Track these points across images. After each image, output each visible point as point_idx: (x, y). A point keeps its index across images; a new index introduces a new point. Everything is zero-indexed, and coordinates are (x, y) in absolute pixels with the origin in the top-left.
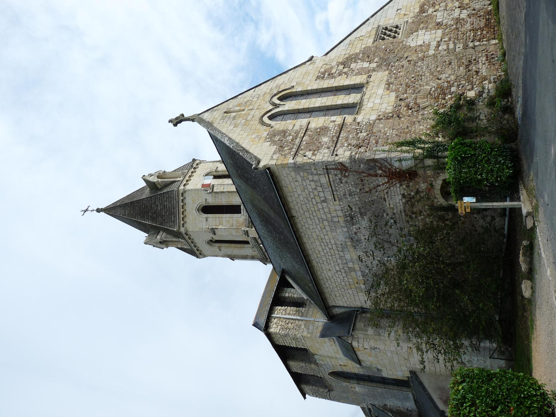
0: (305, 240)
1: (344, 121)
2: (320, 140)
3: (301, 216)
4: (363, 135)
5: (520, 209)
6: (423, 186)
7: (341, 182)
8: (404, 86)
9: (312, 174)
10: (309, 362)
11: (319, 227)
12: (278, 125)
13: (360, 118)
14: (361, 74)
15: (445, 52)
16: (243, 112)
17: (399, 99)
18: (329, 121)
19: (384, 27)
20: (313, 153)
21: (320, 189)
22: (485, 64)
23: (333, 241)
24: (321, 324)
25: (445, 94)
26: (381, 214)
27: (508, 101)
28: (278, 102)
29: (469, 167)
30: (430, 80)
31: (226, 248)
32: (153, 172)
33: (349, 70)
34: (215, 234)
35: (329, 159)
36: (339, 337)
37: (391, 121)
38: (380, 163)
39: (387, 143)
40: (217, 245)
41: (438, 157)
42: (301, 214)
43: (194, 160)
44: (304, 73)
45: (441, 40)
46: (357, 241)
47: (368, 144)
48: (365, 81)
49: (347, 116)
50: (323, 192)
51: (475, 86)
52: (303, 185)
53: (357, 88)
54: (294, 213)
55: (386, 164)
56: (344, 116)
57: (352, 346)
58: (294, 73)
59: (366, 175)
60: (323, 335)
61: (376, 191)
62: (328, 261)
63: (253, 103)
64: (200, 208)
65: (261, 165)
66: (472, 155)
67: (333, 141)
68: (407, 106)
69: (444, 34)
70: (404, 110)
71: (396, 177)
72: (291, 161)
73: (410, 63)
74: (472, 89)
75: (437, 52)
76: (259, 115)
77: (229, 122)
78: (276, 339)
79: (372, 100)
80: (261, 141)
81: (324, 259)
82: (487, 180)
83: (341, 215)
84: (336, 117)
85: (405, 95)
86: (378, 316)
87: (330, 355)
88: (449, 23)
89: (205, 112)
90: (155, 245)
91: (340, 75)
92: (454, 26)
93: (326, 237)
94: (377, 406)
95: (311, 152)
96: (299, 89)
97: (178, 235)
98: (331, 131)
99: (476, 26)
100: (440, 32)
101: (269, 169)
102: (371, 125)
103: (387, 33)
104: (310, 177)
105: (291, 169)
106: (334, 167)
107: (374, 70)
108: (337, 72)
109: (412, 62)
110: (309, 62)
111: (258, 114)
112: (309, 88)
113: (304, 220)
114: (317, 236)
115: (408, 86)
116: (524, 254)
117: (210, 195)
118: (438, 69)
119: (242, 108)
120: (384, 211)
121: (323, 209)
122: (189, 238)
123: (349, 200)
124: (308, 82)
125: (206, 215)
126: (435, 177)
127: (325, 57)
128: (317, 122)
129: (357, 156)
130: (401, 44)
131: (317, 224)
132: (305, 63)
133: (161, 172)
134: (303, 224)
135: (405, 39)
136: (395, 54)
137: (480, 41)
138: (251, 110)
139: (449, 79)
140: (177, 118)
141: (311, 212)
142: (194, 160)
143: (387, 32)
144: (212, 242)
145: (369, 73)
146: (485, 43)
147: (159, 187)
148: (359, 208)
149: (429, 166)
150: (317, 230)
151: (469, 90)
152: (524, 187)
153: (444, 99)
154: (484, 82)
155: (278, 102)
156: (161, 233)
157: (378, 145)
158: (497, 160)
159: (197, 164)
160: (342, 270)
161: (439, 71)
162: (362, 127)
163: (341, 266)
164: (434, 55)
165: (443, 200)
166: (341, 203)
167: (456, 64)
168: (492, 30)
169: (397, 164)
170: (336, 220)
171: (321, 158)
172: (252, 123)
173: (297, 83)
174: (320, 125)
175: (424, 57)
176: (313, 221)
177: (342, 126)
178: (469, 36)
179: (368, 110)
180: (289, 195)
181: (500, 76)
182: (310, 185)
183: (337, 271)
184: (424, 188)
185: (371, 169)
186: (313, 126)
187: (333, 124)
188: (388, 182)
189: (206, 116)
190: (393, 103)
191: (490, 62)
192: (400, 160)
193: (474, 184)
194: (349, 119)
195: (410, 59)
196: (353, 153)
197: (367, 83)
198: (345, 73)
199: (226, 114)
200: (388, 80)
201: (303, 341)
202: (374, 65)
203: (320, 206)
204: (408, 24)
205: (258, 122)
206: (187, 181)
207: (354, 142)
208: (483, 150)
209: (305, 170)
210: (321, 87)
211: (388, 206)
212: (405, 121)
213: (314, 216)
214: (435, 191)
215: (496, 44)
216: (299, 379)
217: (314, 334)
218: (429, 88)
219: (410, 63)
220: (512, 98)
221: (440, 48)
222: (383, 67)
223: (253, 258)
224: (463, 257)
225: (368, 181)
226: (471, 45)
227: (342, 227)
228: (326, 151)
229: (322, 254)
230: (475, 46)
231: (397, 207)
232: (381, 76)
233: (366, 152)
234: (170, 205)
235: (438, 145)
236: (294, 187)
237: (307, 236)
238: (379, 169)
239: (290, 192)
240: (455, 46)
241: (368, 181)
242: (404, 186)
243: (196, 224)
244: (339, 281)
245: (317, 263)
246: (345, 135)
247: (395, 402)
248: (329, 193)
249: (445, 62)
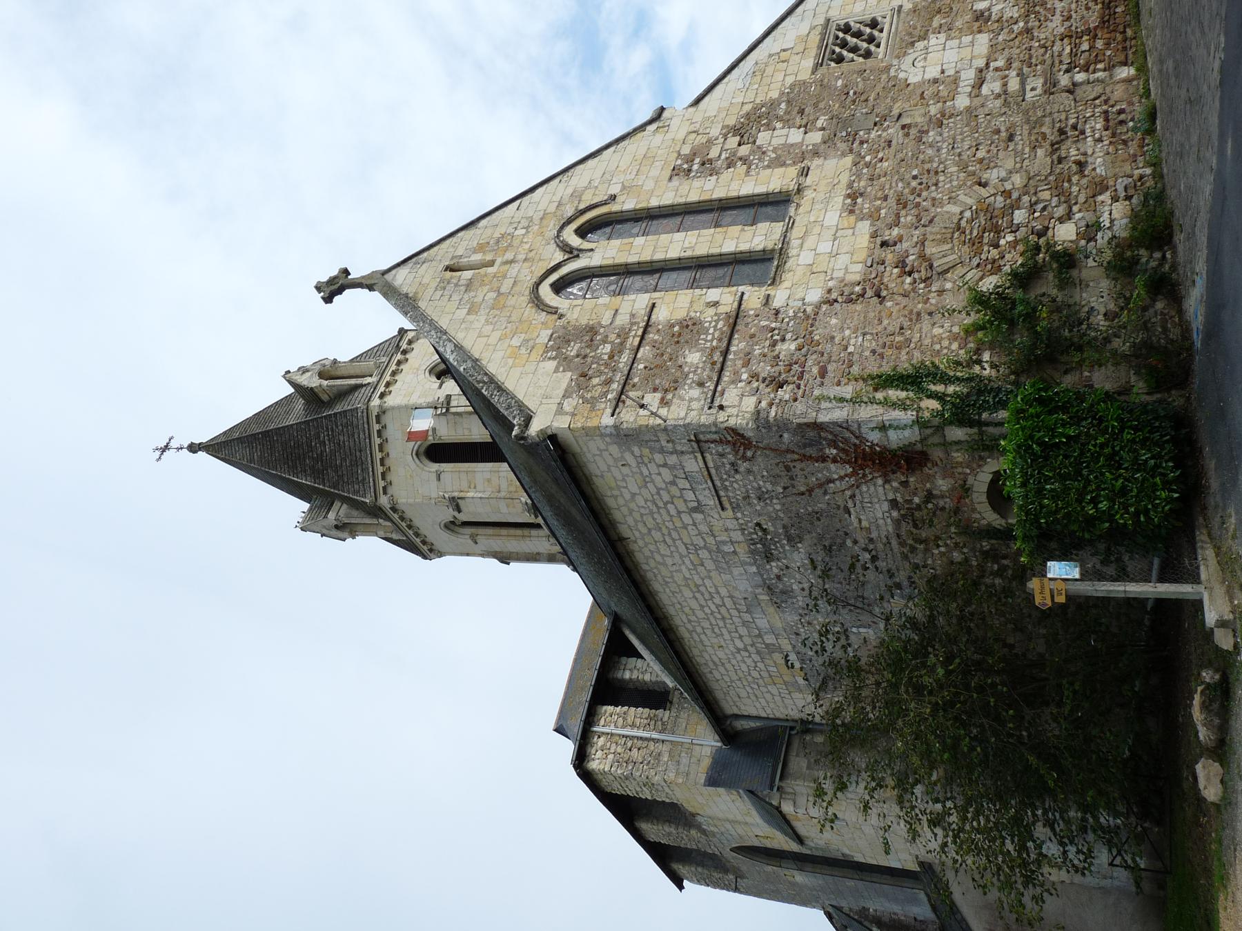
0: (656, 586)
1: (740, 304)
2: (681, 360)
3: (643, 539)
4: (788, 348)
5: (1198, 605)
6: (943, 485)
7: (737, 471)
8: (892, 202)
9: (662, 451)
10: (685, 825)
11: (687, 561)
12: (579, 307)
14: (784, 164)
15: (998, 103)
16: (490, 270)
17: (879, 240)
18: (702, 301)
19: (842, 23)
20: (662, 399)
21: (683, 484)
22: (1100, 140)
23: (723, 592)
24: (707, 751)
25: (998, 231)
26: (839, 541)
27: (1164, 257)
28: (575, 241)
29: (1063, 478)
30: (960, 187)
31: (487, 539)
32: (307, 363)
33: (752, 152)
34: (459, 511)
35: (703, 419)
36: (751, 792)
37: (858, 307)
38: (831, 433)
39: (848, 377)
41: (980, 424)
42: (643, 535)
44: (639, 157)
46: (783, 592)
47: (801, 378)
48: (792, 186)
50: (693, 489)
51: (1075, 209)
52: (641, 473)
53: (772, 205)
54: (624, 531)
55: (848, 435)
56: (741, 289)
57: (781, 812)
58: (617, 156)
59: (796, 457)
60: (713, 781)
61: (825, 493)
62: (716, 630)
63: (516, 242)
64: (422, 449)
65: (535, 428)
66: (1069, 438)
67: (714, 363)
71: (874, 462)
72: (607, 420)
74: (1069, 216)
75: (977, 102)
76: (528, 279)
77: (456, 297)
78: (604, 783)
79: (810, 242)
80: (535, 355)
81: (706, 624)
82: (1111, 519)
83: (741, 538)
84: (719, 290)
85: (896, 232)
86: (840, 742)
87: (731, 817)
89: (398, 265)
90: (325, 531)
91: (730, 164)
92: (1021, 24)
93: (707, 582)
94: (846, 910)
95: (658, 395)
96: (628, 204)
97: (375, 511)
98: (707, 333)
99: (1077, 24)
100: (983, 40)
101: (553, 438)
102: (809, 318)
103: (848, 41)
104: (659, 458)
105: (607, 439)
106: (715, 437)
107: (816, 153)
108: (723, 156)
109: (913, 131)
111: (528, 275)
112: (654, 203)
113: (652, 547)
114: (686, 579)
115: (902, 203)
116: (1205, 707)
117: (443, 418)
118: (980, 155)
119: (489, 257)
120: (846, 534)
121: (694, 524)
122: (402, 518)
123: (758, 508)
124: (649, 185)
125: (435, 467)
126: (975, 466)
127: (692, 110)
128: (675, 304)
129: (773, 414)
130: (884, 76)
131: (681, 556)
132: (642, 128)
133: (327, 363)
134: (648, 553)
135: (895, 62)
136: (870, 104)
137: (1087, 71)
138: (512, 262)
139: (1008, 186)
140: (332, 281)
141: (665, 531)
143: (849, 38)
144: (451, 526)
145: (802, 158)
146: (1100, 75)
147: (325, 398)
148: (784, 527)
149: (958, 443)
150: (683, 567)
151: (1061, 220)
152: (1209, 535)
153: (996, 246)
154: (1100, 198)
155: (575, 241)
156: (337, 504)
157: (826, 381)
158: (1136, 459)
159: (410, 342)
160: (749, 648)
161: (981, 161)
162: (784, 325)
163: (748, 641)
165: (995, 516)
166: (739, 515)
167: (1025, 138)
168: (1119, 37)
169: (874, 437)
170: (728, 548)
171: (682, 414)
172: (511, 301)
173: (624, 187)
174: (680, 314)
176: (673, 549)
177: (735, 319)
178: (1060, 55)
179: (800, 271)
180: (609, 494)
181: (1141, 177)
182: (659, 474)
183: (739, 650)
184: (944, 488)
185: (811, 445)
186: (661, 315)
187: (711, 311)
188: (854, 473)
189: (401, 279)
190: (862, 255)
191: (1114, 135)
192: (883, 428)
193: (1074, 527)
194: (753, 296)
196: (764, 404)
197: (799, 191)
198: (744, 160)
199: (448, 274)
200: (850, 186)
201: (667, 790)
203: (687, 519)
204: (902, 15)
205: (526, 299)
206: (388, 385)
207: (766, 370)
208: (1101, 420)
209: (642, 443)
210: (682, 200)
211: (856, 524)
212: (895, 310)
213: (674, 540)
214: (975, 496)
215: (1128, 81)
216: (663, 856)
217: (692, 776)
218: (956, 209)
219: (907, 135)
220: (1174, 253)
221: (985, 90)
222: (839, 145)
223: (551, 559)
224: (1045, 631)
225: (802, 470)
226: (1064, 80)
227: (743, 564)
228: (696, 392)
229: (700, 614)
230: (1074, 84)
231: (878, 526)
232: (832, 172)
233: (795, 400)
234: (352, 444)
235: (981, 388)
237: (659, 578)
238: (829, 446)
239: (611, 489)
240: (1023, 84)
241: (802, 470)
242: (895, 484)
243: (415, 485)
244: (744, 668)
245: (690, 632)
246: (742, 345)
247: (887, 905)
248: (707, 492)
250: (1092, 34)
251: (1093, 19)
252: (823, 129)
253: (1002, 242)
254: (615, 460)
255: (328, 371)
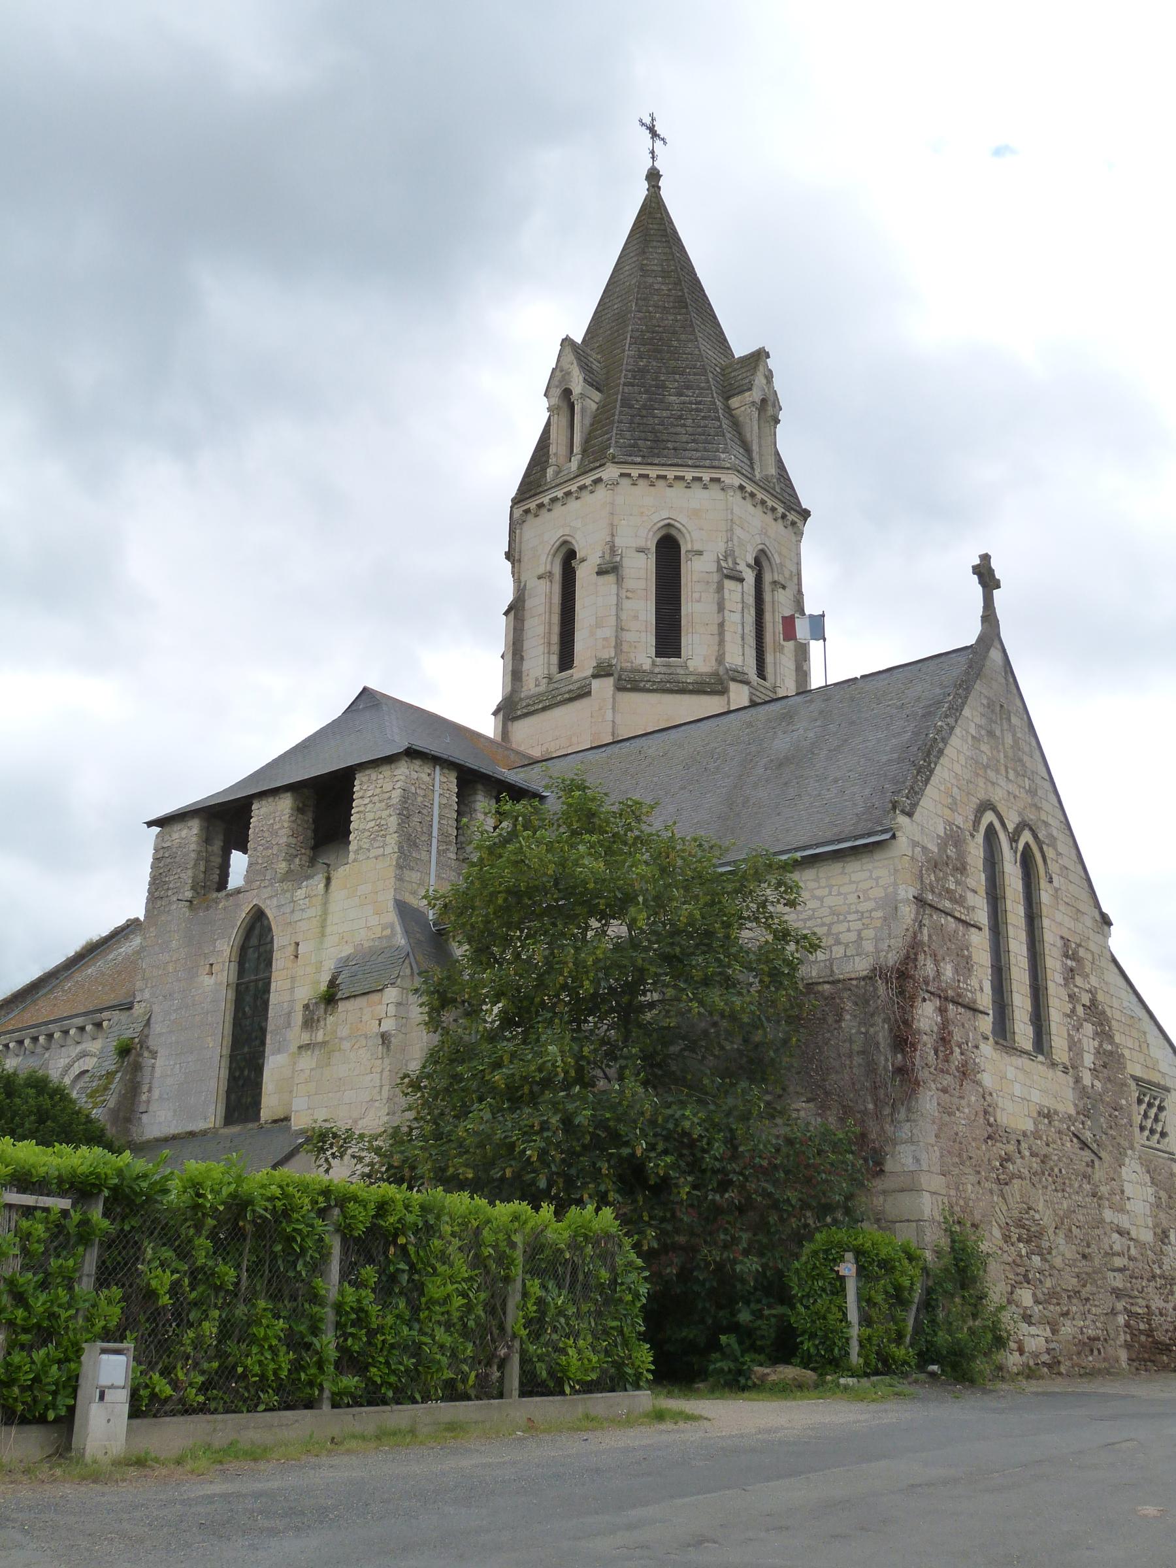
1: (982, 1012)
8: (1045, 1150)
13: (987, 1049)
14: (1070, 1049)
15: (1107, 1247)
17: (1021, 1138)
19: (1165, 1104)
22: (1082, 1333)
25: (1028, 1241)
34: (600, 573)
37: (981, 1121)
40: (557, 570)
43: (806, 514)
45: (1131, 1239)
49: (990, 1019)
51: (1041, 1307)
56: (991, 1012)
64: (674, 532)
68: (1007, 1159)
69: (1142, 1245)
70: (1001, 1149)
73: (1088, 1165)
80: (947, 812)
85: (1027, 1153)
88: (1166, 1260)
91: (1072, 997)
99: (1157, 1320)
100: (1147, 1236)
104: (869, 933)
107: (1078, 1080)
109: (1089, 1169)
110: (1098, 917)
112: (1046, 922)
115: (1044, 1159)
118: (1074, 1228)
139: (1054, 1252)
142: (806, 514)
143: (1154, 1110)
151: (1034, 1295)
154: (1048, 1329)
156: (597, 396)
161: (1070, 1231)
164: (1102, 1221)
173: (1056, 890)
174: (975, 958)
175: (1100, 1198)
177: (974, 1010)
178: (1137, 1304)
182: (849, 930)
191: (1084, 1343)
194: (986, 1024)
195: (1097, 1165)
198: (1073, 1011)
202: (1087, 1079)
210: (1047, 952)
218: (1041, 1207)
219: (1088, 1165)
221: (1115, 1236)
223: (515, 675)
236: (843, 890)
239: (828, 878)
249: (1089, 1247)
250: (1149, 1333)
251: (1159, 1335)
252: (1093, 1086)
253: (1021, 1245)
254: (865, 891)
255: (769, 410)
